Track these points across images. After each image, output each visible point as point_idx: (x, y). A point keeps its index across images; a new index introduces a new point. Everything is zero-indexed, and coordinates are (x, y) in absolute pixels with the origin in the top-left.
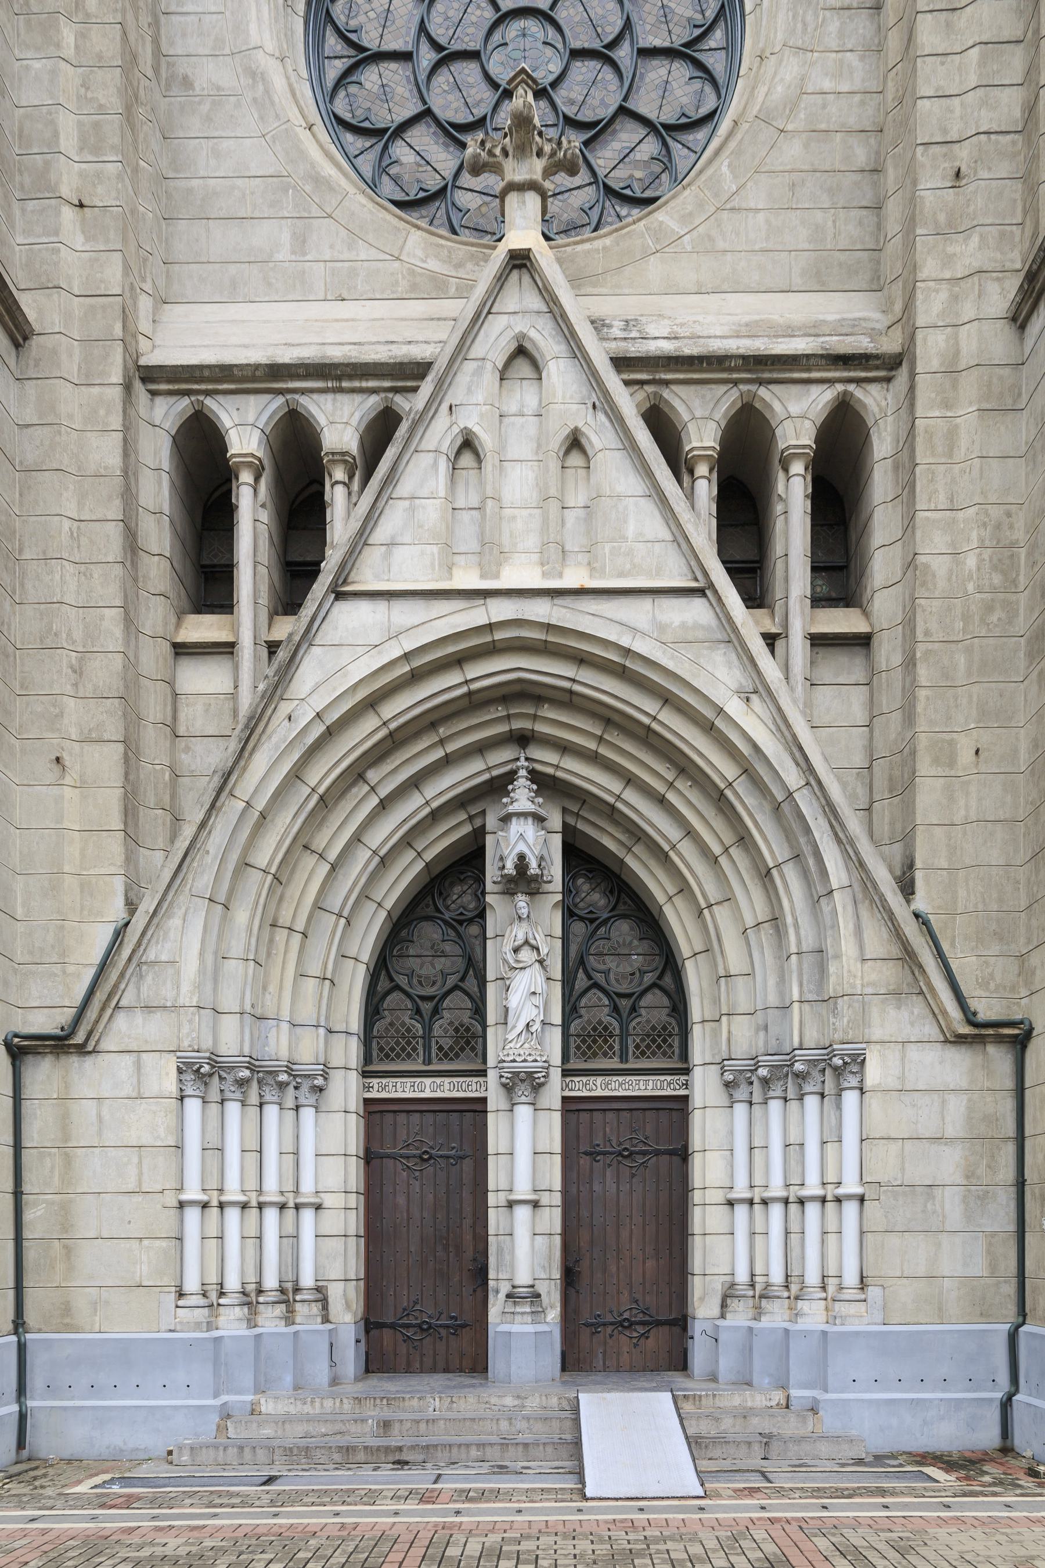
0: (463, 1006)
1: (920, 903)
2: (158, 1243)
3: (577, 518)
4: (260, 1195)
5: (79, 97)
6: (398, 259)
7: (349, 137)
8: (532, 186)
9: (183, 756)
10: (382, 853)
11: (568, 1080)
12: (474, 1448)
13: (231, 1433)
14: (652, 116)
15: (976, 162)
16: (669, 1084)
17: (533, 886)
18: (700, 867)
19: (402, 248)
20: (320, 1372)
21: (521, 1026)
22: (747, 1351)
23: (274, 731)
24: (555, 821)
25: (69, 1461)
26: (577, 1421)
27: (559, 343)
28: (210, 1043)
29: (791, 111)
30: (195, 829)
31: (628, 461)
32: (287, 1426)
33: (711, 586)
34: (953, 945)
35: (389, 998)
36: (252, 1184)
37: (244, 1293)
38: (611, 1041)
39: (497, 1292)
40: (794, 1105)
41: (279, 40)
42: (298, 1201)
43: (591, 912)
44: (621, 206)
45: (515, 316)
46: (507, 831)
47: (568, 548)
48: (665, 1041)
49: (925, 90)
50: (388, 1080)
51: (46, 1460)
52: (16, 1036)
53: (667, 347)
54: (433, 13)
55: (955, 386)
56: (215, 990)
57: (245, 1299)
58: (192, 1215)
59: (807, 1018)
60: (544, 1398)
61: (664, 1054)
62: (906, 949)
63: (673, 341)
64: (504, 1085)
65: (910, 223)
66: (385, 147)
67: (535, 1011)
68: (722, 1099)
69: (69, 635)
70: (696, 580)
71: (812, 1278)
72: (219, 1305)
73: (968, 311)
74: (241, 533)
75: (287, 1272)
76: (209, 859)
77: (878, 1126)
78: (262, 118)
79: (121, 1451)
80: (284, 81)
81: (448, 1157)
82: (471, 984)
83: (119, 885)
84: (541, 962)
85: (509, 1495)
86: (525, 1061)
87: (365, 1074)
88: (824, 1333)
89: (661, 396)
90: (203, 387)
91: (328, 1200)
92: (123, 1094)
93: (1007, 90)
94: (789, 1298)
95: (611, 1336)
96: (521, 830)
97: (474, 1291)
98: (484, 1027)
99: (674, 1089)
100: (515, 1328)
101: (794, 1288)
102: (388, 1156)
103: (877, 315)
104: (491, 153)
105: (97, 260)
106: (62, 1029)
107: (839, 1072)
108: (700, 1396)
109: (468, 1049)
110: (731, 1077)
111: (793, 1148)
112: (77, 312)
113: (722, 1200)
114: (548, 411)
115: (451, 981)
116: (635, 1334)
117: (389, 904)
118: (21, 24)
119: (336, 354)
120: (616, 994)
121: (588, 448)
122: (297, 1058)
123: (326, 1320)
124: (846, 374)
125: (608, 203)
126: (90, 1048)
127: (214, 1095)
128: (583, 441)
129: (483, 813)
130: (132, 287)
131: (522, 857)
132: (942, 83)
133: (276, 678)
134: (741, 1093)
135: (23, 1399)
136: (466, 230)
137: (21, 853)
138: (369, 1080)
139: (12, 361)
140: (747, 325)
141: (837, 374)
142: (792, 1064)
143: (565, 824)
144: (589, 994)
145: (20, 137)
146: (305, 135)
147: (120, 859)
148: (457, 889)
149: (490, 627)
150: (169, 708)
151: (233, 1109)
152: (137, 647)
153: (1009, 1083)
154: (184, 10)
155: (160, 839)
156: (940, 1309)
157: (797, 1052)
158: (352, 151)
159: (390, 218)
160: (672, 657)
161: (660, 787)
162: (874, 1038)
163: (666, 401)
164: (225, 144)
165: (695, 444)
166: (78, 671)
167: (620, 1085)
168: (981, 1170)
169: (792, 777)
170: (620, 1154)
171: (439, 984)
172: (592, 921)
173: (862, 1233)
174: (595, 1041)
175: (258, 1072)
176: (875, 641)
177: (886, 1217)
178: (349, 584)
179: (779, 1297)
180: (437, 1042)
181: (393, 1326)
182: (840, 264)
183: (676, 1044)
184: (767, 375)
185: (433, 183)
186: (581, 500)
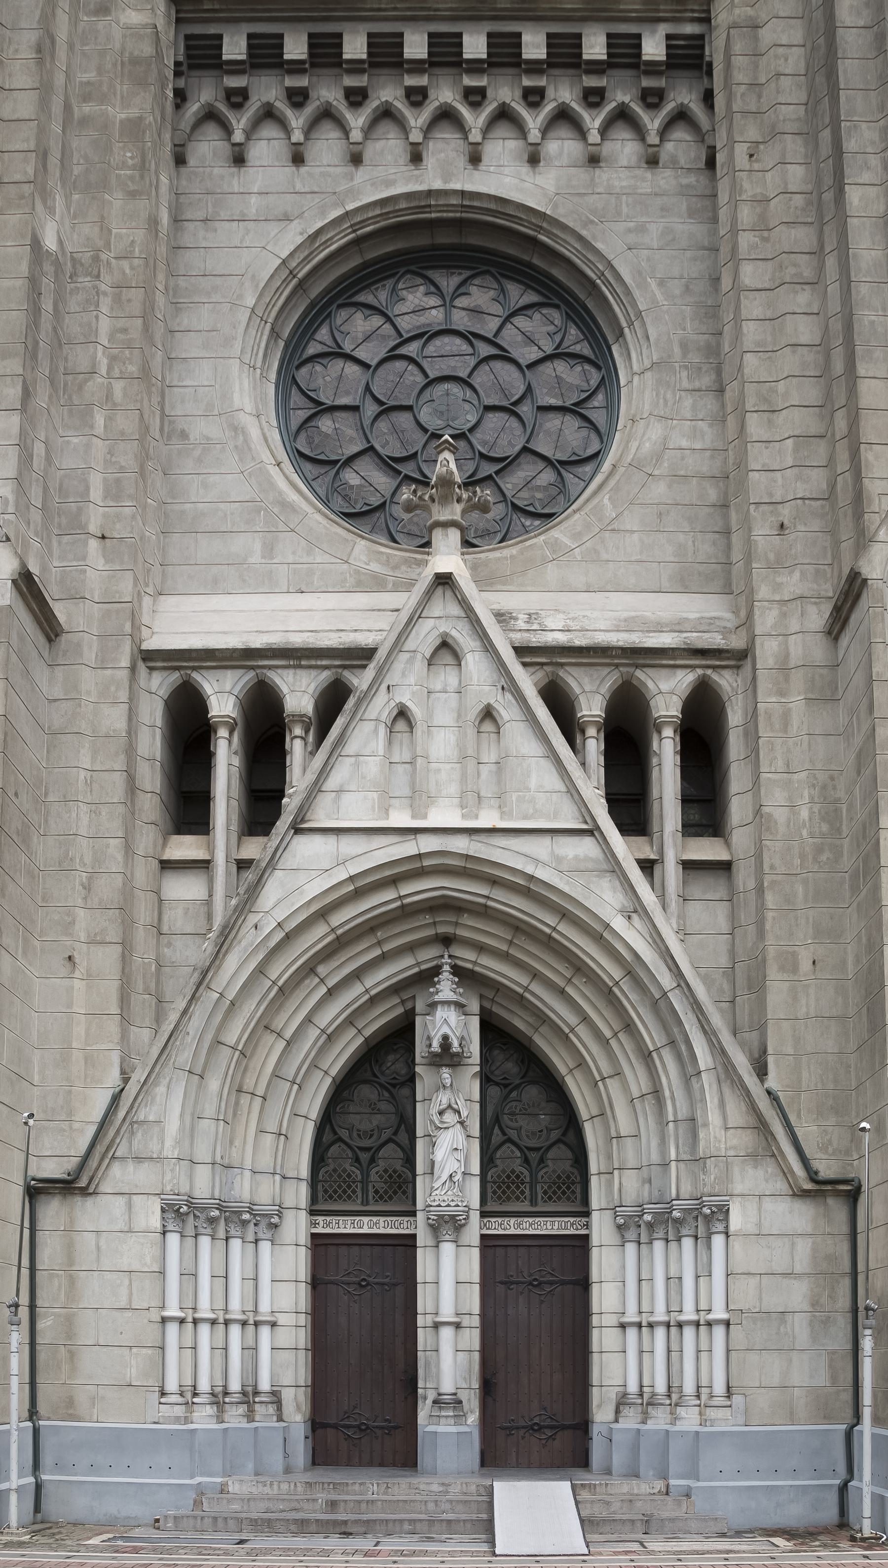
1: (772, 1082)
2: (144, 1351)
3: (490, 771)
4: (226, 1313)
5: (105, 461)
6: (346, 562)
7: (308, 467)
8: (453, 524)
9: (166, 950)
10: (329, 1031)
11: (485, 1220)
12: (407, 1523)
13: (206, 1507)
14: (548, 453)
15: (795, 519)
16: (572, 1225)
17: (455, 1059)
18: (594, 1047)
19: (349, 555)
20: (276, 1461)
21: (445, 1176)
22: (635, 1449)
23: (244, 937)
24: (474, 1006)
25: (75, 1524)
26: (491, 1504)
27: (474, 640)
28: (188, 1188)
29: (657, 461)
30: (178, 1015)
31: (530, 730)
32: (252, 1503)
33: (598, 828)
34: (799, 1116)
35: (332, 1149)
36: (220, 1305)
37: (212, 1394)
38: (522, 1187)
39: (425, 1398)
40: (673, 1245)
41: (256, 402)
42: (257, 1318)
43: (505, 1078)
44: (525, 518)
45: (440, 620)
46: (434, 1015)
47: (482, 794)
48: (568, 1188)
49: (753, 465)
50: (331, 1218)
51: (57, 1523)
52: (33, 1179)
53: (561, 638)
54: (376, 378)
55: (787, 679)
56: (192, 1144)
57: (214, 1399)
58: (172, 1329)
59: (683, 1174)
60: (464, 1485)
61: (568, 1199)
62: (760, 1121)
63: (567, 633)
64: (431, 1226)
65: (748, 558)
66: (337, 473)
67: (457, 1165)
68: (616, 1240)
69: (81, 859)
70: (586, 822)
71: (689, 1388)
72: (193, 1403)
73: (794, 625)
74: (217, 775)
75: (248, 1378)
76: (189, 1039)
77: (739, 1265)
78: (241, 460)
79: (116, 1518)
80: (259, 431)
81: (383, 1284)
82: (403, 1137)
83: (115, 1058)
84: (462, 1123)
85: (435, 1554)
86: (448, 1206)
87: (312, 1213)
88: (697, 1433)
89: (558, 674)
90: (191, 664)
91: (282, 1319)
92: (117, 1228)
93: (816, 470)
94: (670, 1405)
95: (523, 1438)
96: (445, 1016)
97: (406, 1398)
98: (414, 1175)
99: (577, 1229)
100: (440, 1429)
101: (675, 1397)
102: (331, 1282)
103: (728, 615)
104: (421, 498)
105: (114, 577)
106: (69, 1174)
107: (708, 1219)
108: (595, 1485)
109: (400, 1193)
110: (622, 1221)
111: (674, 1281)
112: (96, 615)
113: (615, 1323)
114: (466, 690)
115: (384, 1137)
116: (544, 1437)
117: (334, 1072)
118: (65, 413)
119: (297, 640)
121: (498, 719)
122: (257, 1200)
123: (280, 1419)
124: (704, 662)
125: (515, 516)
126: (91, 1191)
127: (190, 1231)
128: (495, 713)
129: (414, 997)
130: (139, 593)
131: (445, 1038)
132: (767, 461)
133: (246, 896)
134: (631, 1234)
135: (37, 1473)
136: (401, 534)
137: (38, 1031)
139: (46, 654)
140: (625, 620)
141: (697, 662)
142: (671, 1212)
143: (482, 1008)
144: (504, 1147)
145: (60, 490)
146: (274, 471)
147: (116, 1038)
148: (391, 1058)
149: (420, 856)
150: (156, 913)
151: (205, 1242)
152: (133, 866)
153: (845, 1229)
154: (184, 384)
155: (147, 1019)
156: (792, 1413)
157: (674, 1202)
158: (310, 477)
159: (339, 530)
160: (568, 883)
161: (561, 983)
162: (736, 1192)
163: (562, 678)
164: (212, 478)
165: (585, 713)
166: (88, 888)
168: (824, 1300)
169: (666, 980)
170: (531, 1284)
171: (375, 1137)
172: (506, 1086)
173: (728, 1351)
174: (508, 1187)
175: (225, 1212)
176: (734, 868)
177: (747, 1338)
178: (306, 822)
179: (662, 1404)
180: (374, 1187)
181: (335, 1427)
182: (700, 574)
183: (578, 1191)
184: (641, 662)
185: (375, 501)
186: (493, 758)
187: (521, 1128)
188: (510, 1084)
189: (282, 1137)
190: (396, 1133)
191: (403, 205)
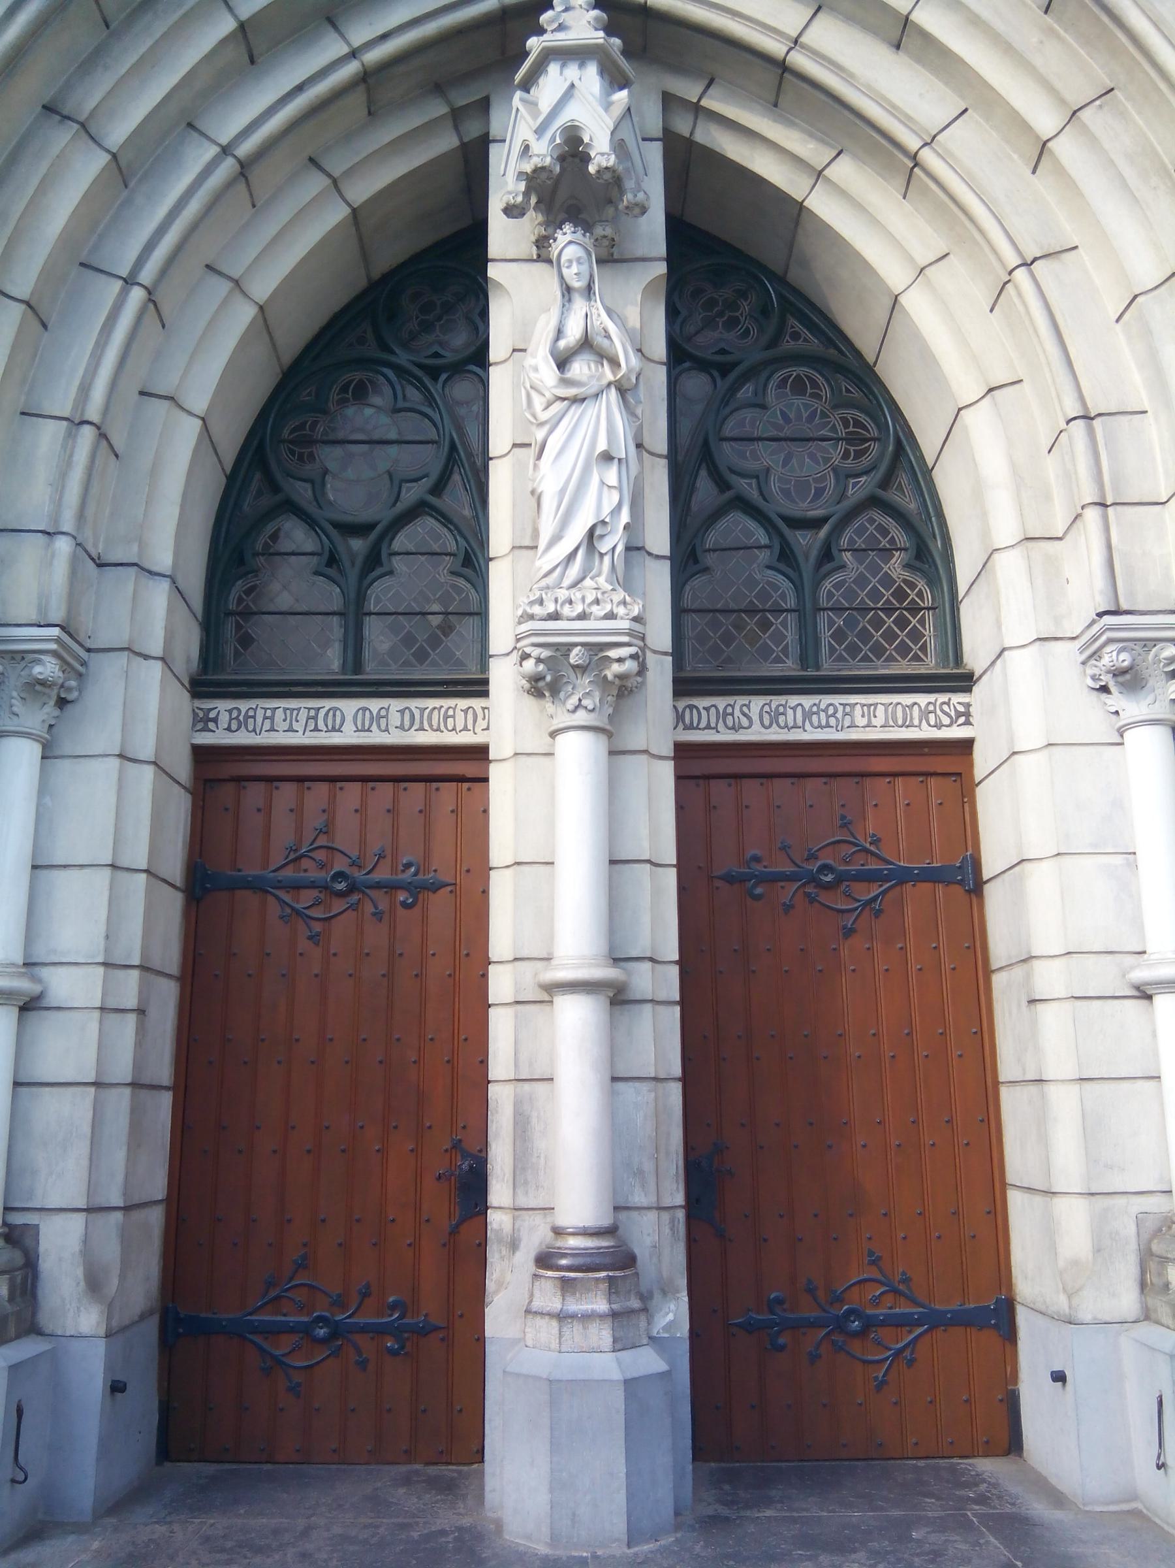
0: (436, 548)
10: (245, 149)
11: (682, 704)
43: (723, 352)
48: (902, 623)
50: (252, 703)
86: (583, 616)
99: (939, 726)
120: (785, 519)
138: (207, 704)
167: (807, 715)
170: (813, 880)
187: (768, 470)
188: (735, 365)
189: (87, 432)
190: (438, 488)
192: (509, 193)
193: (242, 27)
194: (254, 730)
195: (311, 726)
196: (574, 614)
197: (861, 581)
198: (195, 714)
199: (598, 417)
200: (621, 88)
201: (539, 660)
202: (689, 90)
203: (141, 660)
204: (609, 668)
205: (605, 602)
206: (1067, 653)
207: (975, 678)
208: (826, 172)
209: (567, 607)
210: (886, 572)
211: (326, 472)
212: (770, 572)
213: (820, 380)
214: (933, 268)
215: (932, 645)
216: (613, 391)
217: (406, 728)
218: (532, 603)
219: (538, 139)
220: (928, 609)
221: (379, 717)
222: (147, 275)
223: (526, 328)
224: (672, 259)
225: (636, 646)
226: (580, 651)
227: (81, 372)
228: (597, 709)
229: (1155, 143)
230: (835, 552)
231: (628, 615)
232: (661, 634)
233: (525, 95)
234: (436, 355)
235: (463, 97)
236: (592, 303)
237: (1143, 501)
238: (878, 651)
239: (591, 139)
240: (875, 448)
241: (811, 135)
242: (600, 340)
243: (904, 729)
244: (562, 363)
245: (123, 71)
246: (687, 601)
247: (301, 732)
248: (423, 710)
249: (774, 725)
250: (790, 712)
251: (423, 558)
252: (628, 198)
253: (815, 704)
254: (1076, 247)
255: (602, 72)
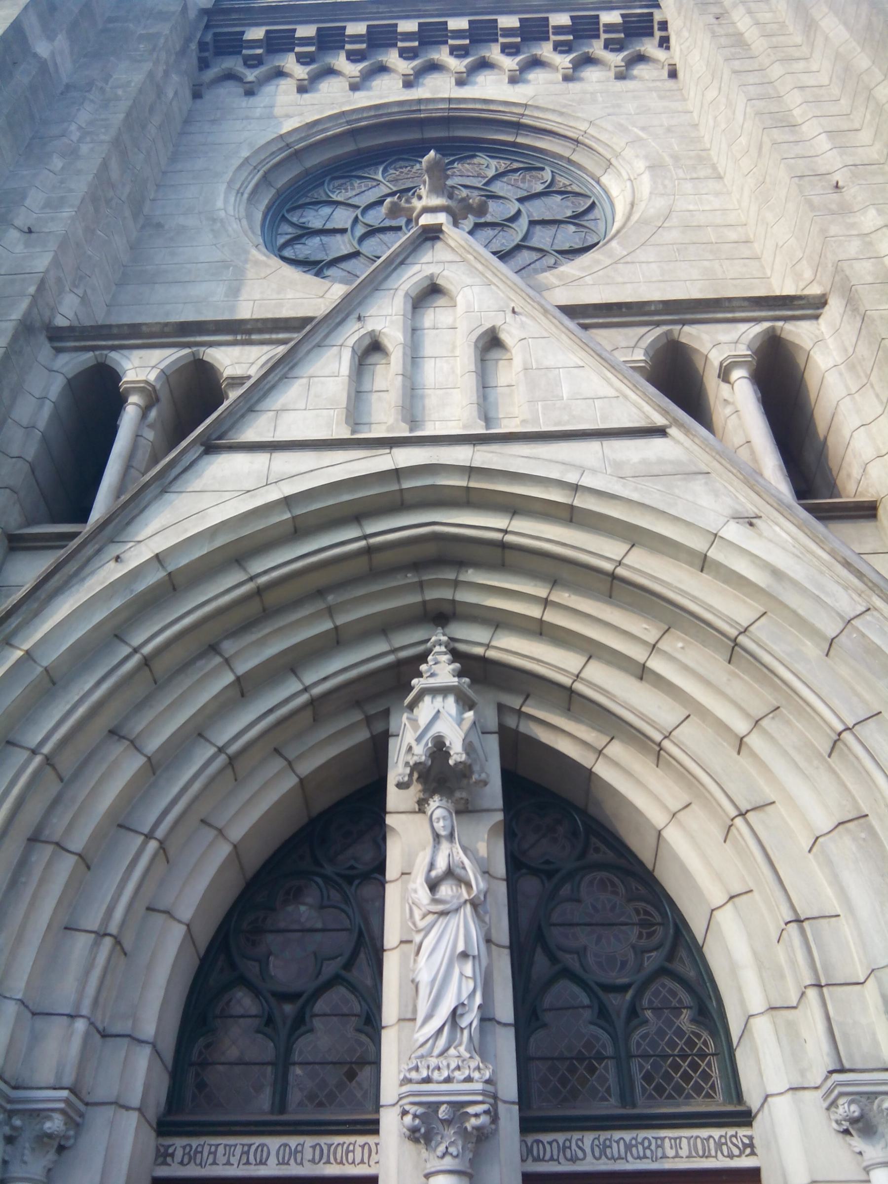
0: (345, 1010)
10: (233, 749)
11: (530, 1139)
16: (719, 1145)
43: (548, 862)
48: (694, 1066)
86: (448, 1080)
90: (110, 343)
99: (731, 1156)
161: (637, 653)
189: (108, 942)
190: (348, 965)
191: (396, 109)
192: (400, 775)
193: (238, 679)
194: (201, 1164)
195: (244, 1160)
196: (442, 1078)
197: (661, 1033)
198: (158, 1150)
199: (458, 926)
200: (470, 709)
201: (415, 1116)
202: (514, 702)
203: (123, 1111)
204: (468, 1120)
205: (464, 1068)
206: (814, 1101)
207: (753, 1115)
208: (605, 751)
209: (436, 1072)
210: (678, 1026)
211: (270, 954)
212: (592, 1027)
213: (616, 880)
214: (682, 813)
215: (719, 1084)
216: (468, 907)
217: (317, 1161)
218: (410, 1070)
219: (417, 744)
220: (713, 1055)
221: (296, 1151)
222: (160, 833)
223: (410, 860)
224: (508, 805)
225: (488, 1103)
226: (446, 1108)
227: (109, 898)
228: (461, 1155)
229: (813, 740)
230: (638, 1010)
231: (481, 1078)
232: (509, 1088)
233: (410, 716)
234: (352, 868)
235: (372, 710)
236: (454, 845)
237: (849, 981)
238: (679, 1090)
239: (450, 744)
240: (660, 930)
241: (593, 728)
242: (458, 871)
243: (704, 1159)
244: (433, 886)
245: (162, 708)
246: (532, 1050)
247: (236, 1165)
248: (329, 1146)
249: (603, 1157)
250: (615, 1145)
251: (335, 1019)
252: (475, 777)
253: (633, 1138)
254: (774, 803)
255: (457, 701)
